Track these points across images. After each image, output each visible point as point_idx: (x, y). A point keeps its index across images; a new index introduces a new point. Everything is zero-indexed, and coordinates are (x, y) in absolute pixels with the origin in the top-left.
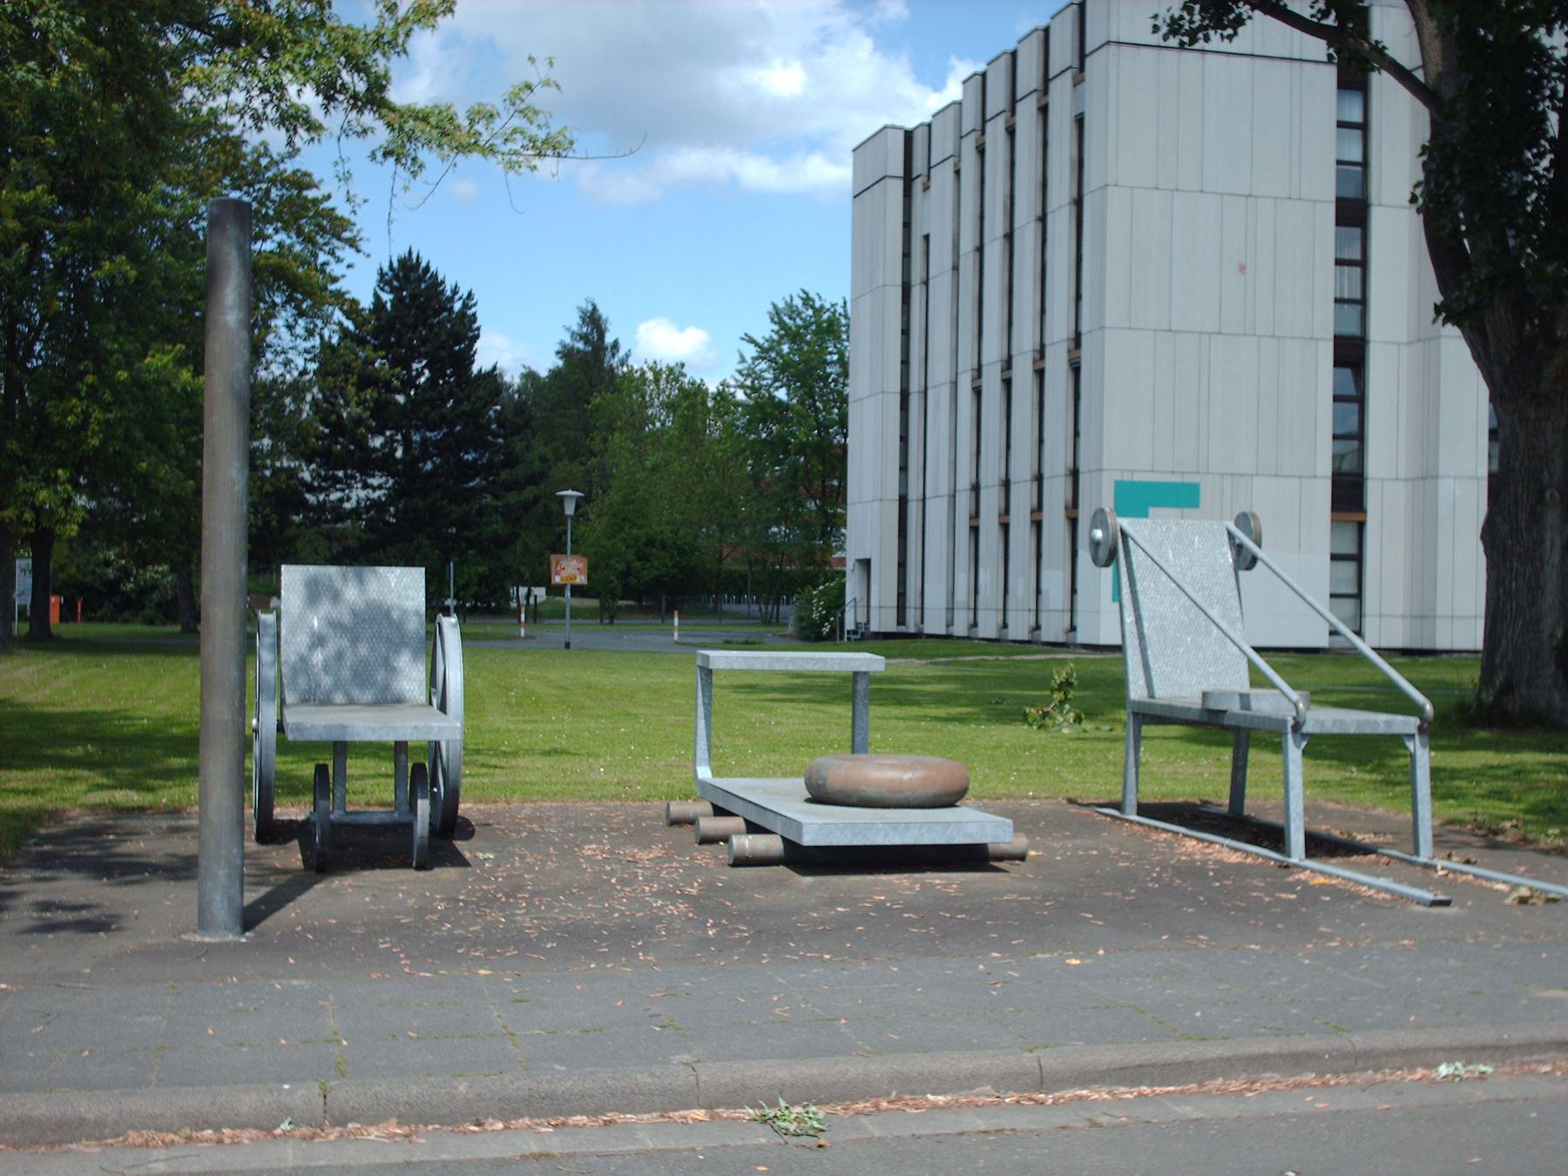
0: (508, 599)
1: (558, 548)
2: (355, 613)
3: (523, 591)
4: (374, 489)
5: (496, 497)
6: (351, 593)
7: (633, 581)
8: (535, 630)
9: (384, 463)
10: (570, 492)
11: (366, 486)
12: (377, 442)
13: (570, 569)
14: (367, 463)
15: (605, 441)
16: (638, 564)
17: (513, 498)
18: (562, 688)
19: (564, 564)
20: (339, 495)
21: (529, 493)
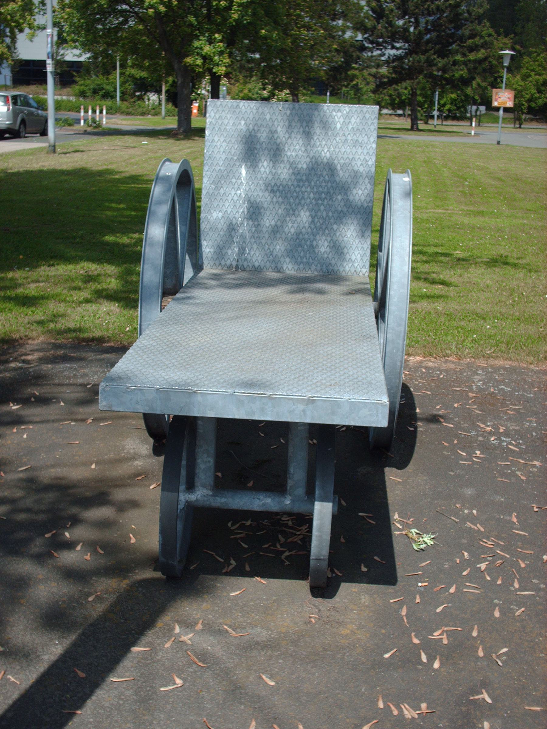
0: (466, 111)
1: (495, 85)
2: (296, 173)
3: (474, 108)
4: (397, 49)
5: (464, 55)
6: (295, 150)
7: (533, 105)
8: (480, 130)
9: (404, 35)
10: (507, 52)
11: (393, 47)
12: (401, 23)
13: (503, 98)
14: (395, 35)
15: (523, 27)
16: (537, 95)
17: (472, 56)
18: (499, 179)
19: (500, 94)
20: (379, 52)
21: (481, 54)
